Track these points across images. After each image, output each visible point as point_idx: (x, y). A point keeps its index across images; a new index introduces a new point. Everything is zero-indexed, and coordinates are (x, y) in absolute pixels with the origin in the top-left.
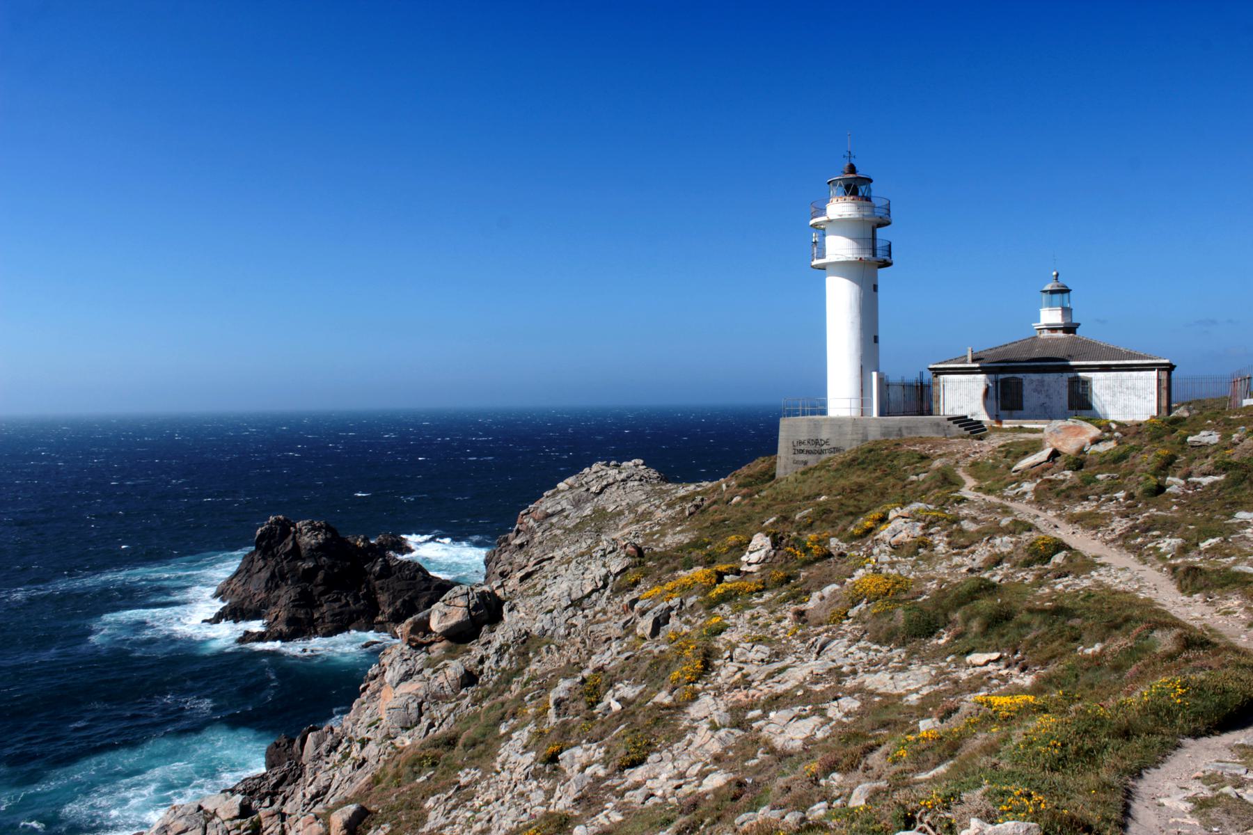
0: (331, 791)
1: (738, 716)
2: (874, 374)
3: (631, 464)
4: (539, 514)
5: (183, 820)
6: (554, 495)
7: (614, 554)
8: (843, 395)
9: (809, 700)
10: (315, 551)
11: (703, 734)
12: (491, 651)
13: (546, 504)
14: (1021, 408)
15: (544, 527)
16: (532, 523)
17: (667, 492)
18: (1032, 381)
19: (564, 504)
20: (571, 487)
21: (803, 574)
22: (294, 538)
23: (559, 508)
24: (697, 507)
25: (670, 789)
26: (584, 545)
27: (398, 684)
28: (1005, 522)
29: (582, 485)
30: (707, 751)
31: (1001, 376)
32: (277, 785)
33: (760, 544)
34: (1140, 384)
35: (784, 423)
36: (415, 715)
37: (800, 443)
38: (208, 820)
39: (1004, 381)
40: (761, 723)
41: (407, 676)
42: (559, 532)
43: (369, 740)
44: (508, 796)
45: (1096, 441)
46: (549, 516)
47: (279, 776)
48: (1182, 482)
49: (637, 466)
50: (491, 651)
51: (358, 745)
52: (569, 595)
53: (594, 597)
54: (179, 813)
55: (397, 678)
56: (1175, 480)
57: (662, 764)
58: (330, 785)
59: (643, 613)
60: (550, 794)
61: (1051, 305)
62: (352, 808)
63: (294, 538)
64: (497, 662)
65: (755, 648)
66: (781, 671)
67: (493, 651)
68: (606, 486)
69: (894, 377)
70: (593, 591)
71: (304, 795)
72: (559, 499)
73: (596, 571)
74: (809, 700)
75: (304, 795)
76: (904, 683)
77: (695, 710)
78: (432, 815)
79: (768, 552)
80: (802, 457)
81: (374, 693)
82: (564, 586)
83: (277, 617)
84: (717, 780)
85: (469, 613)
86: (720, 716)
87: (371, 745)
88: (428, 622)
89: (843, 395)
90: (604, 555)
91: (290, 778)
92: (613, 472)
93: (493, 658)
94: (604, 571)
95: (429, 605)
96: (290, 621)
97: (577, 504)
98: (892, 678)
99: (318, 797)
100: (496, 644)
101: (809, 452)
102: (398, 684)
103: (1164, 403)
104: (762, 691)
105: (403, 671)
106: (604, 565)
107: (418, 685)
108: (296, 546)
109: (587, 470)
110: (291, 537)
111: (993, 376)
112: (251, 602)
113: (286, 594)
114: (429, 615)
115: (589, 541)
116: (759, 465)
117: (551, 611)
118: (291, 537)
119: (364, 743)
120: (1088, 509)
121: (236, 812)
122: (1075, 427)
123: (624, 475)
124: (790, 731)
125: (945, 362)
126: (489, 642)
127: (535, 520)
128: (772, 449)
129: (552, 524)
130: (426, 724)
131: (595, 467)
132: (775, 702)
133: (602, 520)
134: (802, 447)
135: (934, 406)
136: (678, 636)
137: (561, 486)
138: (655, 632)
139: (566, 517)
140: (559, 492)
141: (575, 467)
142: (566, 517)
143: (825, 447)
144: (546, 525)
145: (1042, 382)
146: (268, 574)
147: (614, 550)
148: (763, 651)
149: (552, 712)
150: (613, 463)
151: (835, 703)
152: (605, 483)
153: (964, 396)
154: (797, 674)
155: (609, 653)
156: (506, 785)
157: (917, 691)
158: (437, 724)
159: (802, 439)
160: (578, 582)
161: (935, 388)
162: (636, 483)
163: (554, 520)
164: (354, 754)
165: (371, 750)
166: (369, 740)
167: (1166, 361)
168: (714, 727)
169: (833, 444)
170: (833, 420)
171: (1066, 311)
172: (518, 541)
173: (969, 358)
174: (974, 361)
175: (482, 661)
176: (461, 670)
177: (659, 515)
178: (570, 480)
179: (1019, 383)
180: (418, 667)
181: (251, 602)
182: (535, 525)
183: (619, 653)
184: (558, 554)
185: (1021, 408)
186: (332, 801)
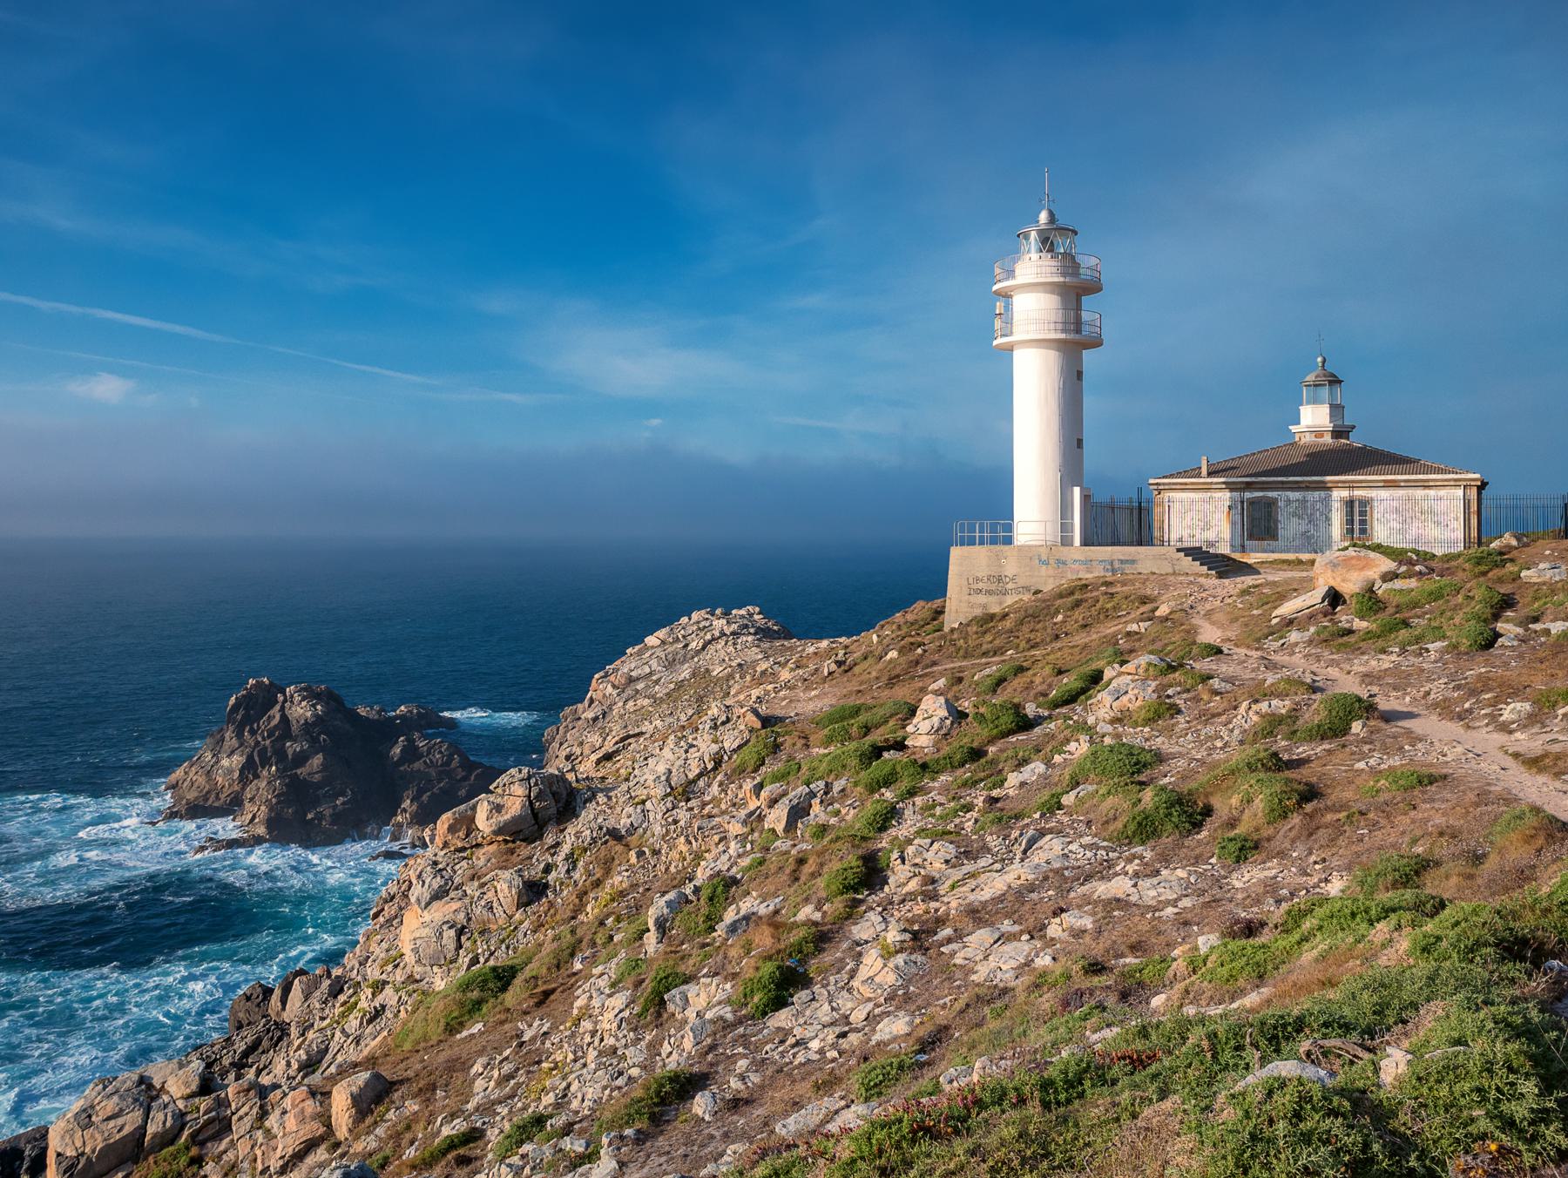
0: (329, 1057)
1: (920, 937)
2: (1077, 490)
3: (743, 612)
4: (618, 679)
5: (115, 1098)
6: (640, 653)
7: (729, 726)
8: (1035, 503)
9: (1022, 911)
10: (307, 727)
11: (872, 960)
12: (560, 858)
13: (628, 665)
14: (1274, 537)
15: (625, 695)
16: (610, 689)
17: (791, 648)
18: (1289, 501)
19: (654, 663)
20: (663, 642)
21: (992, 749)
22: (282, 708)
23: (647, 670)
24: (839, 663)
25: (831, 1038)
26: (683, 718)
27: (428, 904)
28: (1271, 678)
29: (677, 640)
30: (880, 986)
31: (1248, 495)
32: (246, 1054)
33: (933, 709)
34: (1441, 506)
35: (956, 553)
36: (452, 946)
37: (977, 580)
38: (153, 1099)
39: (1252, 502)
40: (954, 946)
41: (438, 895)
42: (646, 702)
43: (385, 983)
44: (592, 1054)
45: (1389, 577)
46: (631, 680)
47: (249, 1040)
48: (1520, 630)
49: (751, 615)
50: (560, 858)
51: (369, 992)
52: (668, 780)
53: (701, 783)
54: (110, 1089)
55: (427, 896)
56: (1509, 626)
57: (815, 1004)
58: (327, 1049)
59: (773, 802)
60: (654, 1048)
61: (1315, 401)
62: (364, 1076)
63: (282, 708)
64: (568, 871)
65: (936, 845)
66: (973, 875)
67: (562, 855)
68: (710, 642)
69: (1101, 497)
70: (700, 775)
71: (289, 1064)
72: (647, 657)
73: (705, 746)
74: (1022, 911)
75: (289, 1064)
76: (1153, 893)
77: (861, 931)
78: (479, 1084)
79: (942, 720)
80: (982, 599)
81: (389, 921)
82: (661, 769)
83: (254, 817)
84: (895, 1027)
85: (531, 803)
86: (893, 936)
87: (388, 990)
88: (473, 820)
89: (1035, 503)
90: (715, 727)
91: (265, 1043)
92: (719, 623)
93: (562, 869)
94: (715, 748)
95: (472, 794)
96: (271, 823)
97: (671, 663)
98: (1135, 885)
99: (309, 1066)
100: (566, 849)
101: (989, 592)
102: (428, 904)
103: (1474, 533)
104: (952, 903)
105: (435, 886)
106: (715, 741)
107: (455, 905)
108: (285, 719)
109: (684, 620)
110: (278, 707)
111: (1236, 494)
112: (217, 798)
113: (263, 789)
114: (474, 808)
115: (690, 712)
116: (920, 609)
117: (643, 802)
118: (278, 707)
119: (379, 987)
120: (1386, 666)
121: (194, 1087)
122: (1359, 558)
123: (734, 627)
124: (994, 959)
125: (1171, 476)
126: (558, 844)
127: (614, 686)
128: (941, 589)
129: (637, 691)
130: (467, 960)
131: (695, 616)
132: (977, 915)
133: (704, 686)
134: (980, 586)
135: (1156, 533)
136: (823, 829)
137: (651, 640)
138: (791, 826)
139: (657, 682)
140: (647, 648)
141: (668, 618)
142: (657, 682)
143: (1010, 586)
144: (629, 692)
145: (1305, 501)
146: (243, 759)
147: (728, 720)
148: (945, 849)
149: (651, 938)
150: (718, 611)
151: (1057, 920)
152: (708, 637)
153: (1199, 515)
154: (994, 885)
155: (725, 858)
156: (588, 1039)
157: (1174, 903)
158: (482, 960)
159: (980, 575)
160: (681, 762)
161: (1157, 510)
162: (750, 638)
163: (640, 686)
164: (363, 1004)
165: (388, 996)
166: (385, 983)
167: (1477, 476)
168: (887, 954)
169: (1022, 582)
170: (1021, 548)
171: (1336, 410)
172: (590, 715)
173: (1204, 471)
174: (1210, 474)
175: (548, 869)
176: (518, 882)
177: (785, 675)
178: (662, 633)
179: (1271, 504)
180: (457, 880)
181: (217, 798)
182: (615, 692)
183: (739, 856)
184: (647, 727)
185: (1274, 537)
186: (333, 1069)
